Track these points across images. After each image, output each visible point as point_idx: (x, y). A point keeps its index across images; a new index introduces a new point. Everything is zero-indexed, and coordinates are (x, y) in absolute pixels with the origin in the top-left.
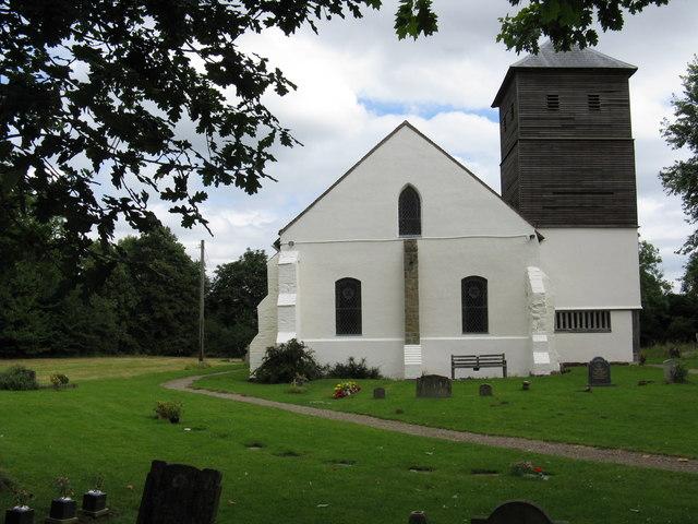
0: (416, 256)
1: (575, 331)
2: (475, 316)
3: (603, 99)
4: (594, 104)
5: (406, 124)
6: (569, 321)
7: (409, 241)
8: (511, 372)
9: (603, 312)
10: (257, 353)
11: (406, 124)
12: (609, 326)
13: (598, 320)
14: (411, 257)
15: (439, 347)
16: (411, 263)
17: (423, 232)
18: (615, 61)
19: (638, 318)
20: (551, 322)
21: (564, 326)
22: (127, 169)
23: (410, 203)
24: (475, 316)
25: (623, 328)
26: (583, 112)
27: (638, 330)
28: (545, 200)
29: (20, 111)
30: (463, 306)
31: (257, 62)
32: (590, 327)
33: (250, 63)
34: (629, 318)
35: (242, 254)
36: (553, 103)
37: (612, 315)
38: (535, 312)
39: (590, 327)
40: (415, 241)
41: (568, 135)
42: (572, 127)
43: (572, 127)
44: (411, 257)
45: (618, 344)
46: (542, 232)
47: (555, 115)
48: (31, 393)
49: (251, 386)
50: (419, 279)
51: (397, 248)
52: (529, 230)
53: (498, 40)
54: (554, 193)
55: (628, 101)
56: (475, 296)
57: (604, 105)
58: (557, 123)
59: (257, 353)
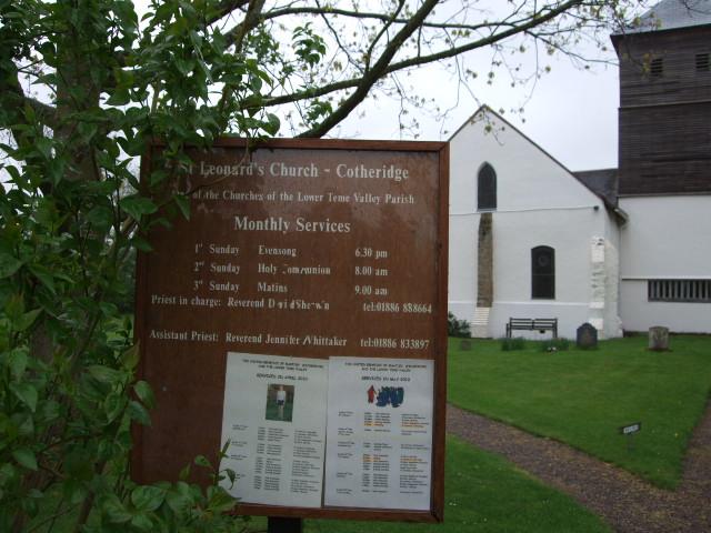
2: (543, 284)
7: (485, 214)
24: (543, 284)
40: (490, 214)
41: (672, 100)
58: (660, 89)
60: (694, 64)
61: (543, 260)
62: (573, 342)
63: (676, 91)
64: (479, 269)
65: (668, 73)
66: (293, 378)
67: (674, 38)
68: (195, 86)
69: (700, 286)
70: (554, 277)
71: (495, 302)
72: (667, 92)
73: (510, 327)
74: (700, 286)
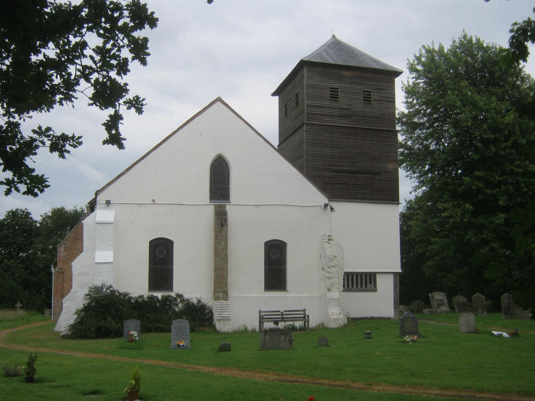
0: (226, 220)
2: (275, 275)
5: (219, 100)
7: (220, 206)
8: (313, 323)
10: (71, 307)
14: (221, 220)
15: (246, 306)
16: (222, 226)
17: (231, 200)
18: (384, 65)
19: (398, 283)
20: (339, 281)
22: (13, 189)
23: (220, 176)
24: (275, 275)
25: (386, 288)
27: (398, 290)
30: (265, 266)
31: (68, 3)
32: (359, 286)
33: (65, 4)
34: (391, 278)
35: (121, 291)
36: (334, 95)
37: (378, 277)
38: (329, 273)
39: (359, 286)
40: (225, 206)
41: (346, 123)
42: (349, 116)
44: (221, 220)
45: (381, 302)
46: (334, 205)
49: (68, 342)
50: (228, 241)
51: (209, 211)
52: (323, 200)
55: (394, 98)
56: (275, 261)
57: (375, 100)
58: (337, 112)
59: (71, 307)
60: (361, 97)
61: (275, 261)
62: (127, 319)
63: (349, 116)
64: (215, 262)
65: (343, 101)
66: (442, 395)
67: (347, 73)
68: (409, 205)
69: (350, 277)
70: (285, 269)
71: (230, 294)
72: (342, 116)
73: (262, 320)
74: (350, 277)
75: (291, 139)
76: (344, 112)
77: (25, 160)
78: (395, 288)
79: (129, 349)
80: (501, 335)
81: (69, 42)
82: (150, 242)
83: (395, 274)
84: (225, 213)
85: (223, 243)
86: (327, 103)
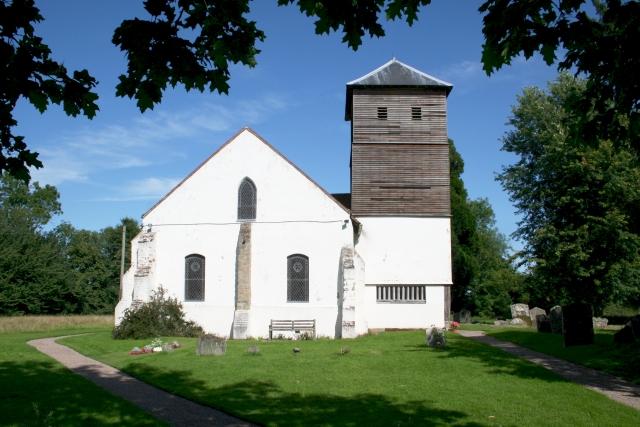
0: (249, 237)
1: (396, 302)
2: (298, 288)
3: (425, 110)
4: (417, 114)
5: (351, 91)
6: (390, 292)
9: (420, 286)
11: (351, 91)
12: (425, 298)
13: (416, 292)
21: (387, 298)
24: (298, 288)
26: (408, 122)
28: (371, 193)
29: (190, 4)
36: (383, 113)
37: (427, 288)
40: (249, 224)
41: (394, 140)
42: (398, 133)
43: (398, 133)
44: (245, 236)
45: (431, 315)
47: (384, 123)
48: (335, 192)
53: (482, 9)
54: (381, 187)
58: (386, 130)
75: (418, 183)
76: (393, 130)
77: (174, 84)
78: (446, 300)
79: (161, 389)
80: (53, 82)
81: (529, 33)
82: (125, 21)
83: (445, 285)
84: (249, 231)
85: (245, 257)
86: (376, 123)
